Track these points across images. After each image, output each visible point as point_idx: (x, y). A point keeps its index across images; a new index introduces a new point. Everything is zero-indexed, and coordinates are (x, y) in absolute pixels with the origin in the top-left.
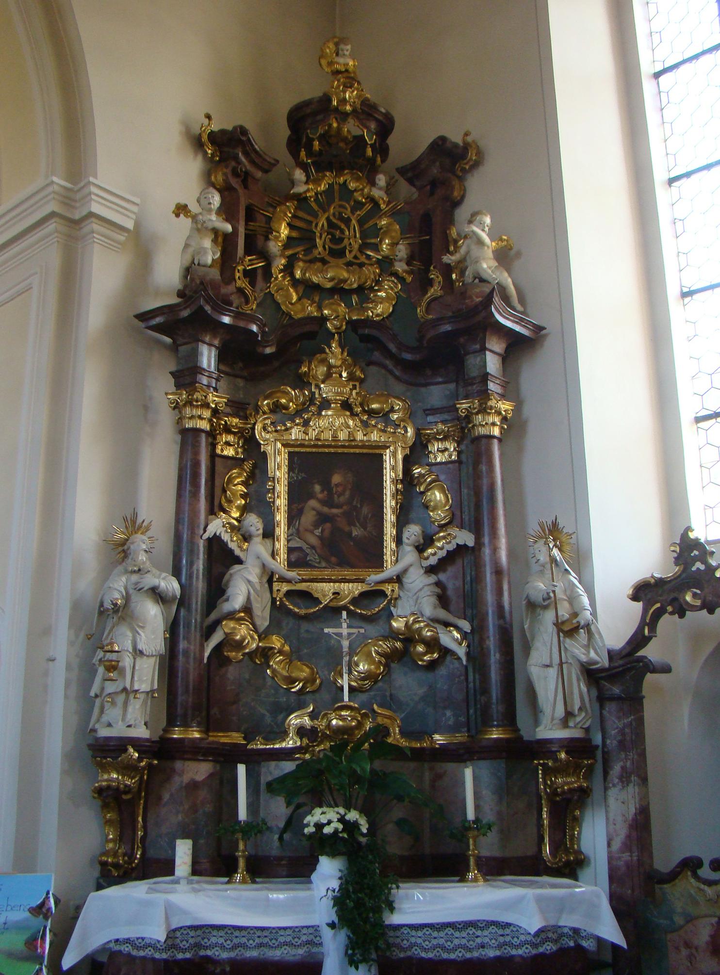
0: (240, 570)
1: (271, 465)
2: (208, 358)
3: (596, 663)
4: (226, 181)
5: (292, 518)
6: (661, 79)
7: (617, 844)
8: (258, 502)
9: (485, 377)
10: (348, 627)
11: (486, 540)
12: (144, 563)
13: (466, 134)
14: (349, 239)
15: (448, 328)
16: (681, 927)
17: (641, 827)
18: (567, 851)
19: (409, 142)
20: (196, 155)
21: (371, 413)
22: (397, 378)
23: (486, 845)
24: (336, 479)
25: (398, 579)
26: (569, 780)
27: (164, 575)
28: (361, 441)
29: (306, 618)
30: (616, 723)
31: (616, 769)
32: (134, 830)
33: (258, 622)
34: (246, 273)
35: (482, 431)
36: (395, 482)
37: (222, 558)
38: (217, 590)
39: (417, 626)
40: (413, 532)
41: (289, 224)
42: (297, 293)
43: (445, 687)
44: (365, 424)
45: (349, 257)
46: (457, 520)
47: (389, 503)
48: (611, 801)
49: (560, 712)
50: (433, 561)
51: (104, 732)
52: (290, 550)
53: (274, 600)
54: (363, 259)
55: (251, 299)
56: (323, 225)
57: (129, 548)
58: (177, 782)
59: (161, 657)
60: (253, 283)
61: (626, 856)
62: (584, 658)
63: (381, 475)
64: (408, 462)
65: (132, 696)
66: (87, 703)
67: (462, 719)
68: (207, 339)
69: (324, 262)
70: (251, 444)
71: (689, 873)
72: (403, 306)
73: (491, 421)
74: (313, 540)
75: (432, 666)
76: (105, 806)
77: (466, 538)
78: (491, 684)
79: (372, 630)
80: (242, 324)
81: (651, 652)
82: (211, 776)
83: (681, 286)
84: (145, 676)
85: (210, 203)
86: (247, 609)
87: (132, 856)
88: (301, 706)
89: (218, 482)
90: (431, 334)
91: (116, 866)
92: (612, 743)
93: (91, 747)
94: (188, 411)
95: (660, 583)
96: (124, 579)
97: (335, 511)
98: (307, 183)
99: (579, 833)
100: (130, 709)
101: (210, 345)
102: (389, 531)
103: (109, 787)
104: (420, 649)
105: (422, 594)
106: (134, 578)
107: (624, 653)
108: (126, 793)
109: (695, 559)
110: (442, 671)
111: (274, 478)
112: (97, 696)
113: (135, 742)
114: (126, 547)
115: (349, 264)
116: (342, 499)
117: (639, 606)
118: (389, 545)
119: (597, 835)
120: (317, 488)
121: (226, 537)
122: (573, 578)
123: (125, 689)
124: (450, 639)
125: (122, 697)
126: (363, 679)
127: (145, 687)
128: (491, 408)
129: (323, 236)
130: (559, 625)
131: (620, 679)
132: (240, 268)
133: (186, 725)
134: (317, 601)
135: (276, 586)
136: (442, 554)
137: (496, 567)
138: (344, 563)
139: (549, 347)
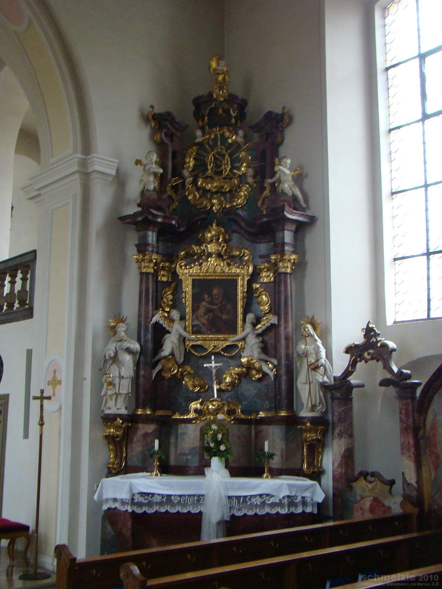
0: (169, 336)
1: (184, 285)
2: (152, 237)
3: (328, 383)
4: (162, 139)
5: (195, 309)
6: (390, 71)
7: (336, 465)
8: (176, 304)
9: (283, 244)
10: (215, 363)
11: (282, 322)
12: (123, 337)
13: (284, 108)
14: (225, 165)
15: (265, 219)
16: (359, 501)
17: (348, 457)
18: (314, 467)
19: (255, 113)
20: (146, 126)
21: (232, 258)
22: (246, 239)
23: (276, 462)
24: (215, 291)
25: (244, 339)
26: (312, 435)
27: (133, 341)
28: (227, 273)
29: (201, 357)
30: (338, 410)
31: (337, 431)
32: (122, 454)
33: (178, 360)
34: (173, 187)
35: (283, 270)
36: (243, 292)
37: (160, 332)
38: (158, 345)
39: (253, 362)
40: (250, 317)
41: (194, 159)
42: (199, 193)
43: (266, 390)
44: (229, 265)
45: (225, 174)
46: (273, 311)
47: (240, 304)
48: (335, 445)
49: (310, 405)
50: (260, 331)
51: (107, 412)
52: (193, 326)
53: (186, 350)
54: (231, 175)
55: (175, 200)
56: (211, 159)
57: (117, 330)
58: (140, 432)
59: (132, 378)
60: (176, 192)
61: (340, 470)
62: (321, 380)
63: (236, 289)
64: (250, 282)
65: (119, 396)
66: (98, 400)
67: (273, 405)
68: (151, 229)
69: (212, 178)
70: (175, 275)
71: (363, 478)
72: (251, 200)
73: (286, 265)
74: (204, 321)
75: (259, 380)
76: (109, 443)
77: (274, 320)
78: (283, 391)
79: (232, 362)
80: (167, 221)
81: (353, 380)
82: (155, 430)
83: (392, 189)
84: (125, 387)
85: (151, 160)
86: (172, 354)
87: (121, 464)
88: (197, 399)
89: (159, 294)
90: (259, 222)
91: (114, 469)
92: (336, 419)
93: (102, 418)
94: (143, 264)
95: (356, 346)
96: (115, 344)
97: (214, 307)
98: (203, 136)
99: (322, 459)
100: (118, 402)
101: (153, 231)
102: (240, 317)
103: (109, 435)
104: (254, 372)
105: (254, 347)
106: (119, 344)
107: (341, 378)
108: (118, 438)
109: (372, 336)
110: (265, 383)
111: (186, 291)
112: (104, 396)
113: (121, 416)
114: (115, 329)
115: (224, 179)
116: (218, 301)
117: (348, 356)
118: (240, 322)
119: (329, 460)
120: (206, 296)
121: (161, 322)
122: (319, 343)
123: (116, 393)
124: (268, 368)
125: (115, 396)
126: (228, 386)
127: (125, 392)
128: (286, 260)
129: (212, 164)
130: (309, 366)
131: (340, 390)
132: (170, 185)
133: (144, 408)
134: (206, 350)
135: (187, 343)
136: (264, 328)
137: (286, 336)
138: (219, 332)
139: (319, 223)
